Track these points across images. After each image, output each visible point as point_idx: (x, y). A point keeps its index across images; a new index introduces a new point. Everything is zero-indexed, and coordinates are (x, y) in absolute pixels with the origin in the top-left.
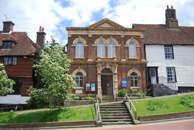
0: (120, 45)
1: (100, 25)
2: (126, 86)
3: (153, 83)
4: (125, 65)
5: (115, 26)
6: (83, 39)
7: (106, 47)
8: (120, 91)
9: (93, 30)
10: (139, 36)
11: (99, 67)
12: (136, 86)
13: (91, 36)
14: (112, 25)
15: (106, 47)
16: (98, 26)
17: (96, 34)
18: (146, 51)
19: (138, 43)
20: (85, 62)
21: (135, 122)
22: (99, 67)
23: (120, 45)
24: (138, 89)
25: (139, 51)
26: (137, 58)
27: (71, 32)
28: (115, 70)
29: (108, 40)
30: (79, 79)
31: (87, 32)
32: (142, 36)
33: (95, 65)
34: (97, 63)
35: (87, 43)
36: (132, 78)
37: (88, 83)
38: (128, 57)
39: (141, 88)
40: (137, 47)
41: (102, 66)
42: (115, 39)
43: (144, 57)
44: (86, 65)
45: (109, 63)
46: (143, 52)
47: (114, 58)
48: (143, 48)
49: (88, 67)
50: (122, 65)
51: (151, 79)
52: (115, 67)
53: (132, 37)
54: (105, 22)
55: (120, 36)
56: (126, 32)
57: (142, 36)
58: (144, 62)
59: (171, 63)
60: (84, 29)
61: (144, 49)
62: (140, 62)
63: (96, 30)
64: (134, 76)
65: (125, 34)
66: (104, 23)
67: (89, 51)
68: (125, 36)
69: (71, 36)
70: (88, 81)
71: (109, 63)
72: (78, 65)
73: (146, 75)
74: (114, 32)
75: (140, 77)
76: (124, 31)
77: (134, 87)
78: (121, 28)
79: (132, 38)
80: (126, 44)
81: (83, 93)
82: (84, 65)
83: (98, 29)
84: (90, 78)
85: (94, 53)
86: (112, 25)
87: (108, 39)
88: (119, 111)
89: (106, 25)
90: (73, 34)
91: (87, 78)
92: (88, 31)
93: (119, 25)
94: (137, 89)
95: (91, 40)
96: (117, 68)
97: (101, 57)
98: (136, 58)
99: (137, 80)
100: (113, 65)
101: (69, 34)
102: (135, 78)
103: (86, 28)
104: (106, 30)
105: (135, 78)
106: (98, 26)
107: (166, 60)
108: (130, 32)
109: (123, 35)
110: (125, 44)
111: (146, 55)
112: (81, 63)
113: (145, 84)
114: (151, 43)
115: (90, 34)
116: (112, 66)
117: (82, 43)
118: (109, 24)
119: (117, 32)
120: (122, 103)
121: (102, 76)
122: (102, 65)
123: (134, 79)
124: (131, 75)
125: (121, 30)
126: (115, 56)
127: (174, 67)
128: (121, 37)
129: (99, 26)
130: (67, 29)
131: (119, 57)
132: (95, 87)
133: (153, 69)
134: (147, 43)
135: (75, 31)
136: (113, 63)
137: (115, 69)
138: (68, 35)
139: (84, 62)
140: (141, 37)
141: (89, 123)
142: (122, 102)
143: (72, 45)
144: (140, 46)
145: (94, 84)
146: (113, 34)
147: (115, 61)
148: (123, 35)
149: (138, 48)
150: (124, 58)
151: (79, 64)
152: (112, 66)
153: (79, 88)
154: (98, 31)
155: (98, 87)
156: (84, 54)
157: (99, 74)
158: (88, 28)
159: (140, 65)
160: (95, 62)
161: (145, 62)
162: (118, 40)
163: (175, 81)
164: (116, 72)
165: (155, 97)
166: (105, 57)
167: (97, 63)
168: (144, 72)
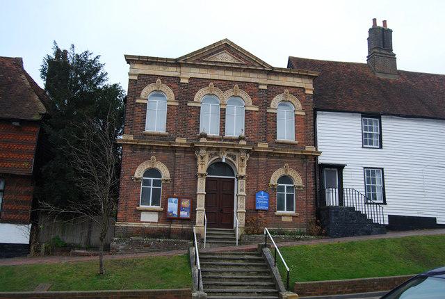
1: (210, 55)
5: (245, 61)
9: (194, 66)
11: (202, 158)
12: (290, 208)
13: (187, 81)
14: (240, 58)
16: (205, 57)
18: (318, 125)
19: (299, 106)
22: (202, 158)
24: (293, 217)
27: (137, 66)
29: (230, 93)
31: (178, 69)
34: (198, 149)
35: (177, 99)
36: (282, 189)
40: (296, 115)
41: (211, 156)
45: (228, 149)
51: (327, 195)
52: (243, 160)
53: (286, 90)
55: (257, 84)
56: (273, 78)
57: (310, 90)
58: (312, 152)
59: (373, 158)
61: (312, 121)
63: (204, 67)
64: (286, 185)
66: (220, 50)
69: (136, 78)
71: (228, 149)
72: (150, 150)
73: (316, 184)
75: (299, 187)
77: (285, 212)
80: (272, 106)
84: (178, 183)
89: (225, 57)
95: (185, 92)
100: (237, 154)
101: (132, 72)
103: (176, 60)
107: (364, 149)
108: (281, 78)
110: (268, 105)
115: (186, 74)
118: (233, 54)
119: (252, 75)
121: (208, 180)
123: (286, 193)
127: (382, 169)
128: (261, 87)
133: (333, 169)
136: (238, 151)
138: (129, 74)
140: (307, 92)
143: (137, 101)
152: (234, 158)
153: (150, 207)
156: (167, 125)
157: (202, 175)
158: (181, 61)
161: (315, 152)
162: (252, 95)
163: (382, 202)
164: (244, 173)
166: (217, 134)
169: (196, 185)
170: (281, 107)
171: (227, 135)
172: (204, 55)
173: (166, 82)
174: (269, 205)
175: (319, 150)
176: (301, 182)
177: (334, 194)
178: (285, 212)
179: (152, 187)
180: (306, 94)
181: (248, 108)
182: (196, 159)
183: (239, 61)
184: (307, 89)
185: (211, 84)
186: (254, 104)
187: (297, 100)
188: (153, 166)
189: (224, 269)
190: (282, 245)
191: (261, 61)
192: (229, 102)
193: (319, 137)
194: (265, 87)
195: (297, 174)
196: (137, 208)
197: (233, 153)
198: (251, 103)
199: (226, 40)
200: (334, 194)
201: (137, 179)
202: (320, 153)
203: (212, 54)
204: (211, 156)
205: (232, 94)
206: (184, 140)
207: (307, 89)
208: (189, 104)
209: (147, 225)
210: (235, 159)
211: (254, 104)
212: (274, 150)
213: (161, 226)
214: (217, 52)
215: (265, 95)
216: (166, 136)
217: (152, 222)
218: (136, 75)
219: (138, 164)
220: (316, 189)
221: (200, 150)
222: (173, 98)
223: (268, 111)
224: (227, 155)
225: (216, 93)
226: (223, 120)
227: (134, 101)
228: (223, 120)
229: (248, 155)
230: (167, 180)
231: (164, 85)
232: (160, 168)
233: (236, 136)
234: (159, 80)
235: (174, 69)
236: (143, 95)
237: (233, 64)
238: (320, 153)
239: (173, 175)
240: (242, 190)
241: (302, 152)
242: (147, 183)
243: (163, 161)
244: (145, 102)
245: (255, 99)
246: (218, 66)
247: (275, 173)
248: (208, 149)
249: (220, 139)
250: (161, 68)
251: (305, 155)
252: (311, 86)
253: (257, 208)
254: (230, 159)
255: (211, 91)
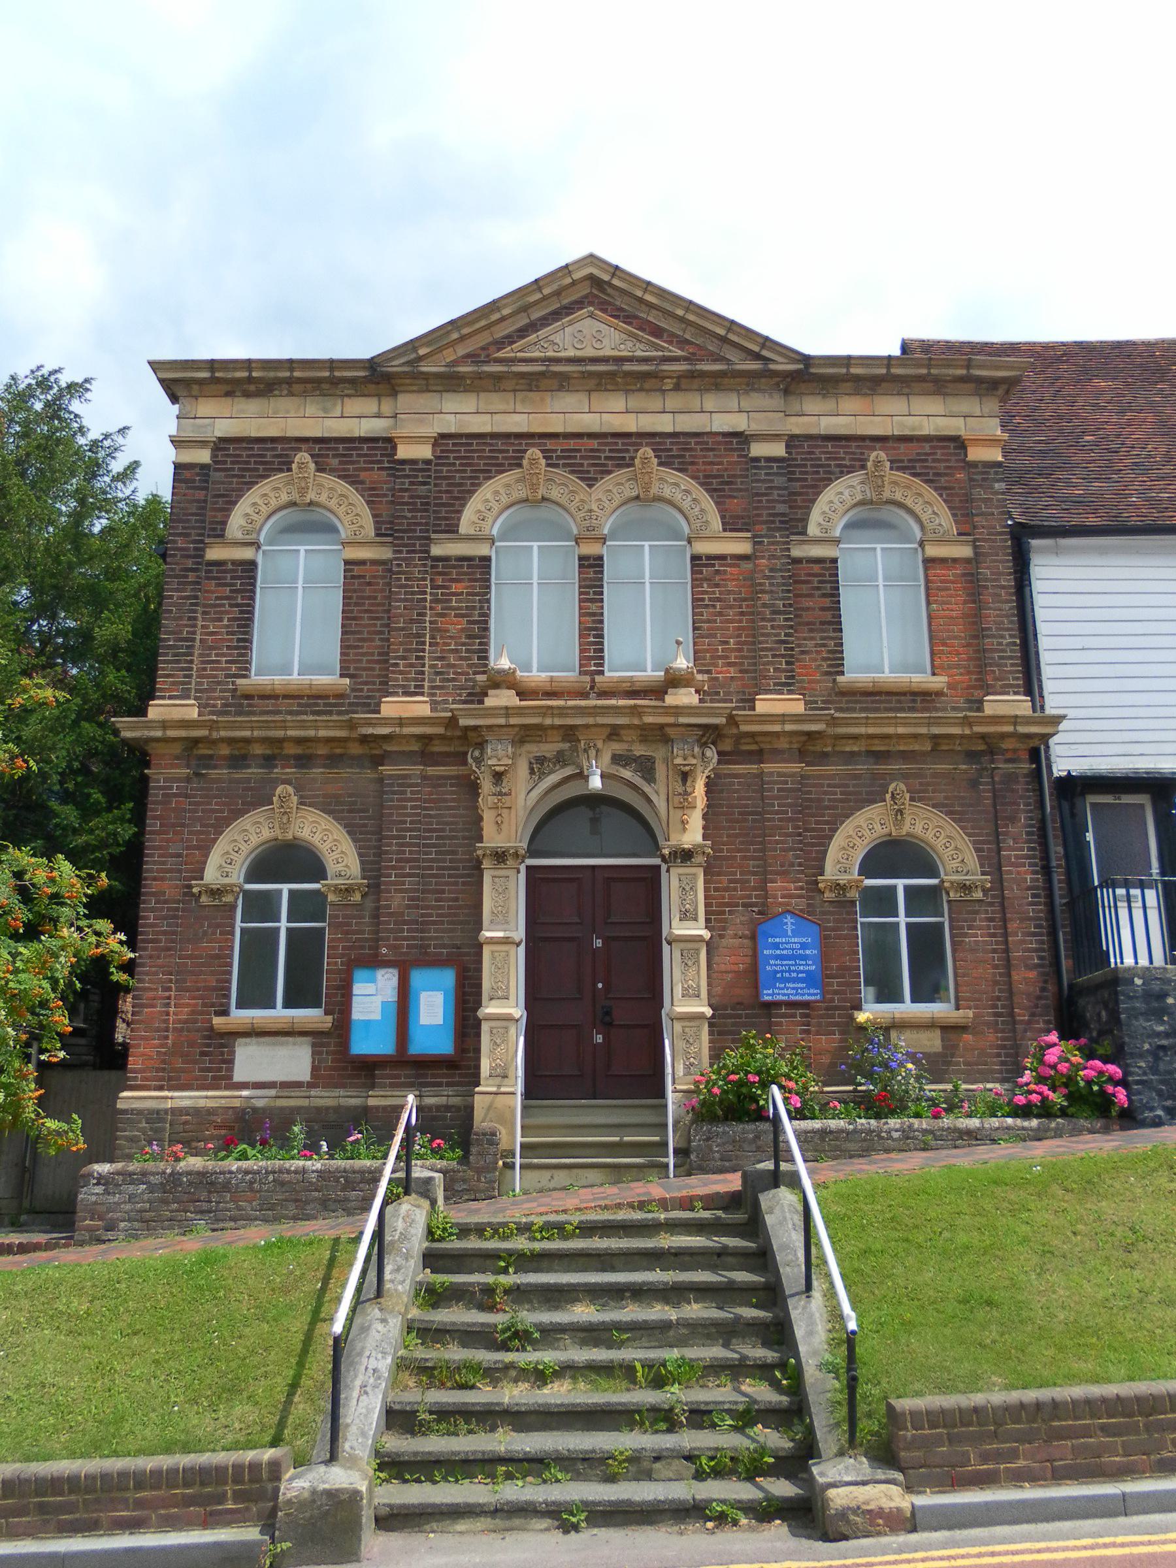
0: (739, 546)
1: (523, 332)
2: (811, 995)
3: (1129, 961)
4: (802, 755)
5: (682, 343)
6: (343, 487)
7: (591, 566)
8: (732, 1058)
9: (451, 382)
10: (958, 443)
11: (498, 777)
12: (925, 991)
13: (425, 452)
14: (657, 332)
15: (591, 566)
16: (500, 344)
17: (480, 424)
18: (1040, 601)
19: (945, 520)
20: (352, 725)
21: (839, 1498)
22: (498, 777)
23: (739, 546)
24: (949, 1029)
25: (956, 605)
26: (939, 682)
27: (206, 407)
28: (676, 815)
30: (283, 924)
31: (387, 406)
32: (992, 442)
33: (460, 758)
34: (474, 739)
35: (386, 530)
36: (883, 901)
37: (374, 962)
38: (836, 663)
39: (988, 1016)
40: (929, 562)
41: (539, 767)
42: (686, 482)
43: (1012, 667)
44: (356, 760)
45: (614, 733)
46: (999, 611)
47: (674, 681)
48: (1000, 567)
49: (380, 780)
50: (759, 756)
51: (1105, 918)
52: (685, 776)
53: (878, 455)
54: (579, 304)
55: (741, 439)
56: (812, 405)
57: (992, 442)
58: (1015, 720)
60: (352, 381)
61: (1008, 581)
62: (966, 722)
63: (496, 383)
64: (900, 883)
65: (796, 426)
66: (568, 310)
67: (399, 607)
68: (792, 441)
69: (203, 456)
70: (376, 942)
71: (614, 733)
72: (269, 761)
73: (1047, 870)
74: (674, 401)
75: (965, 888)
76: (786, 392)
77: (908, 1008)
78: (757, 357)
79: (878, 463)
80: (813, 530)
81: (319, 1078)
82: (334, 760)
83: (498, 378)
84: (396, 901)
85: (456, 626)
86: (657, 332)
87: (607, 482)
88: (658, 1312)
90: (224, 428)
91: (369, 904)
92: (394, 393)
93: (732, 325)
94: (930, 1025)
96: (699, 789)
97: (536, 675)
98: (923, 679)
99: (291, 892)
100: (658, 753)
101: (189, 434)
102: (918, 899)
103: (372, 364)
104: (592, 383)
105: (918, 899)
106: (500, 344)
108: (850, 404)
109: (775, 437)
110: (795, 525)
111: (1044, 643)
112: (300, 741)
113: (1026, 978)
114: (1092, 520)
116: (646, 768)
117: (330, 529)
118: (629, 318)
119: (711, 401)
120: (733, 1201)
121: (537, 880)
122: (541, 760)
123: (902, 920)
124: (869, 867)
125: (748, 382)
126: (682, 663)
128: (758, 450)
129: (510, 340)
130: (167, 385)
131: (724, 672)
132: (357, 1014)
133: (1127, 799)
134: (1052, 516)
135: (253, 406)
136: (659, 735)
137: (686, 805)
138: (177, 442)
139: (340, 725)
140: (976, 454)
141: (188, 1501)
142: (732, 1182)
144: (965, 551)
145: (448, 977)
146: (664, 424)
147: (678, 710)
148: (775, 437)
149: (951, 574)
150: (788, 685)
151: (290, 749)
152: (646, 768)
153: (280, 1014)
154: (496, 401)
155: (490, 1009)
156: (345, 648)
157: (500, 857)
158: (396, 367)
159: (971, 756)
160: (452, 722)
161: (1028, 721)
162: (717, 487)
164: (693, 834)
165: (1157, 1123)
166: (569, 675)
167: (474, 739)
168: (1018, 831)
169: (479, 905)
170: (856, 533)
171: (612, 674)
172: (501, 332)
173: (334, 462)
174: (821, 979)
175: (1049, 711)
176: (972, 860)
177: (1138, 914)
178: (908, 1008)
179: (902, 920)
180: (974, 465)
181: (704, 548)
182: (473, 788)
183: (657, 348)
184: (978, 441)
185: (534, 452)
186: (732, 525)
187: (930, 493)
188: (284, 827)
189: (531, 1317)
190: (665, 1160)
191: (749, 333)
192: (505, 535)
193: (1047, 643)
194: (778, 450)
195: (951, 828)
196: (217, 1021)
197: (639, 750)
198: (716, 524)
199: (592, 259)
200: (1138, 914)
201: (215, 893)
202: (1057, 720)
203: (533, 327)
204: (539, 767)
205: (521, 492)
206: (420, 707)
207: (978, 441)
208: (436, 550)
209: (261, 1100)
210: (649, 776)
211: (732, 525)
212: (833, 722)
213: (325, 1098)
214: (556, 315)
215: (780, 481)
216: (341, 696)
217: (285, 1085)
218: (202, 444)
219: (220, 826)
220: (1050, 895)
221: (481, 745)
222: (370, 530)
223: (796, 552)
224: (617, 759)
225: (555, 494)
226: (593, 608)
227: (199, 553)
228: (593, 608)
229: (711, 753)
230: (349, 890)
231: (328, 480)
232: (316, 840)
233: (651, 673)
234: (303, 457)
235: (369, 405)
236: (236, 523)
237: (630, 359)
238: (1057, 720)
239: (373, 866)
240: (687, 916)
241: (966, 722)
242: (262, 906)
243: (331, 806)
244: (247, 554)
245: (736, 505)
246: (491, 375)
247: (846, 830)
248: (526, 735)
249: (584, 695)
250: (312, 407)
251: (983, 737)
252: (993, 428)
253: (767, 996)
254: (627, 774)
255: (534, 487)
